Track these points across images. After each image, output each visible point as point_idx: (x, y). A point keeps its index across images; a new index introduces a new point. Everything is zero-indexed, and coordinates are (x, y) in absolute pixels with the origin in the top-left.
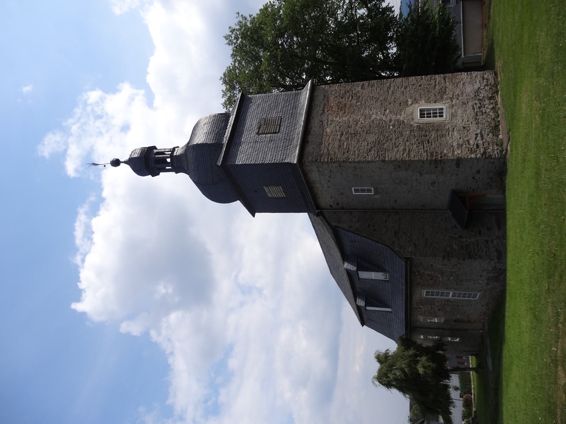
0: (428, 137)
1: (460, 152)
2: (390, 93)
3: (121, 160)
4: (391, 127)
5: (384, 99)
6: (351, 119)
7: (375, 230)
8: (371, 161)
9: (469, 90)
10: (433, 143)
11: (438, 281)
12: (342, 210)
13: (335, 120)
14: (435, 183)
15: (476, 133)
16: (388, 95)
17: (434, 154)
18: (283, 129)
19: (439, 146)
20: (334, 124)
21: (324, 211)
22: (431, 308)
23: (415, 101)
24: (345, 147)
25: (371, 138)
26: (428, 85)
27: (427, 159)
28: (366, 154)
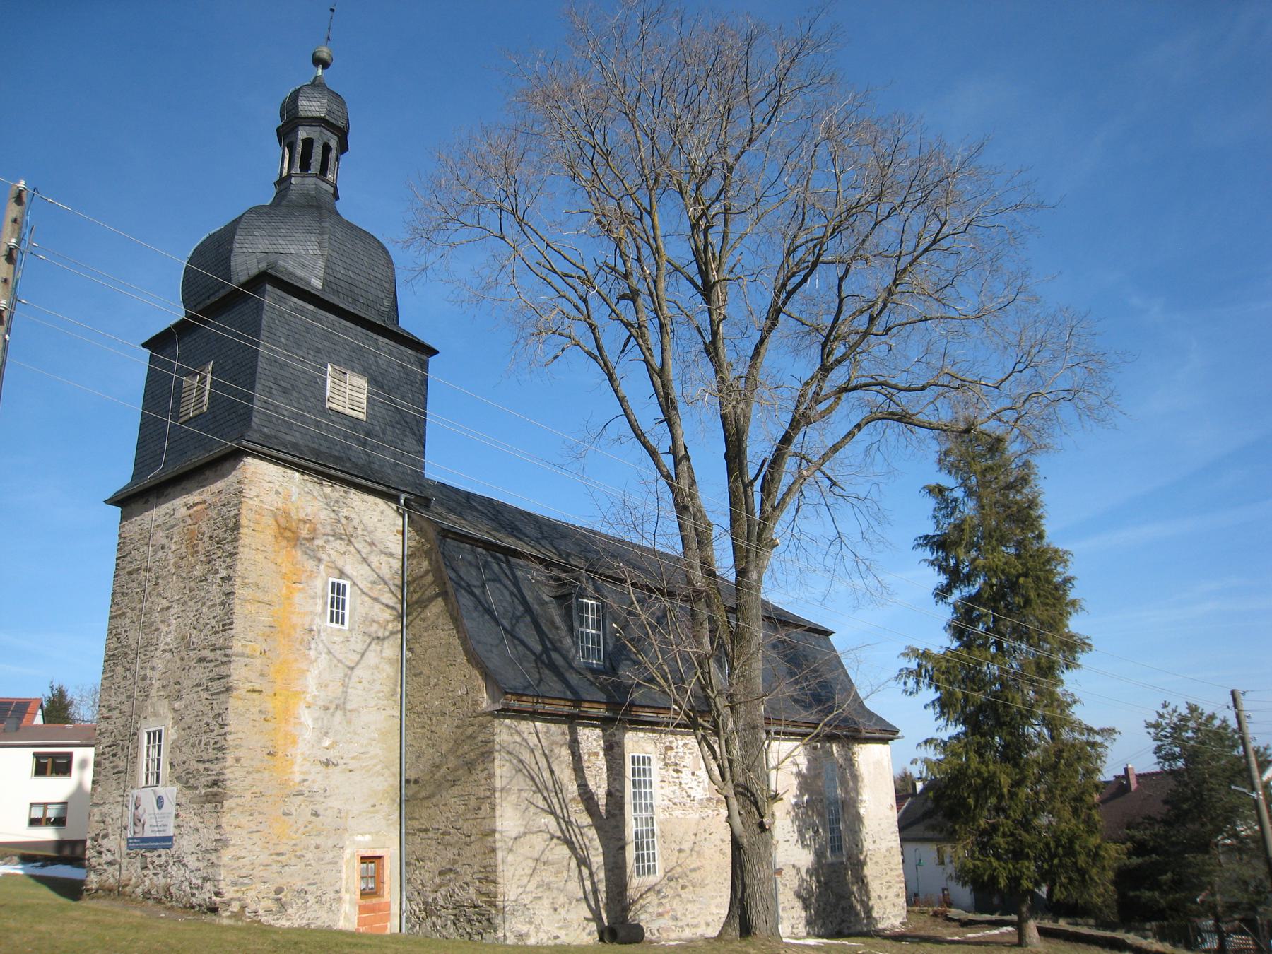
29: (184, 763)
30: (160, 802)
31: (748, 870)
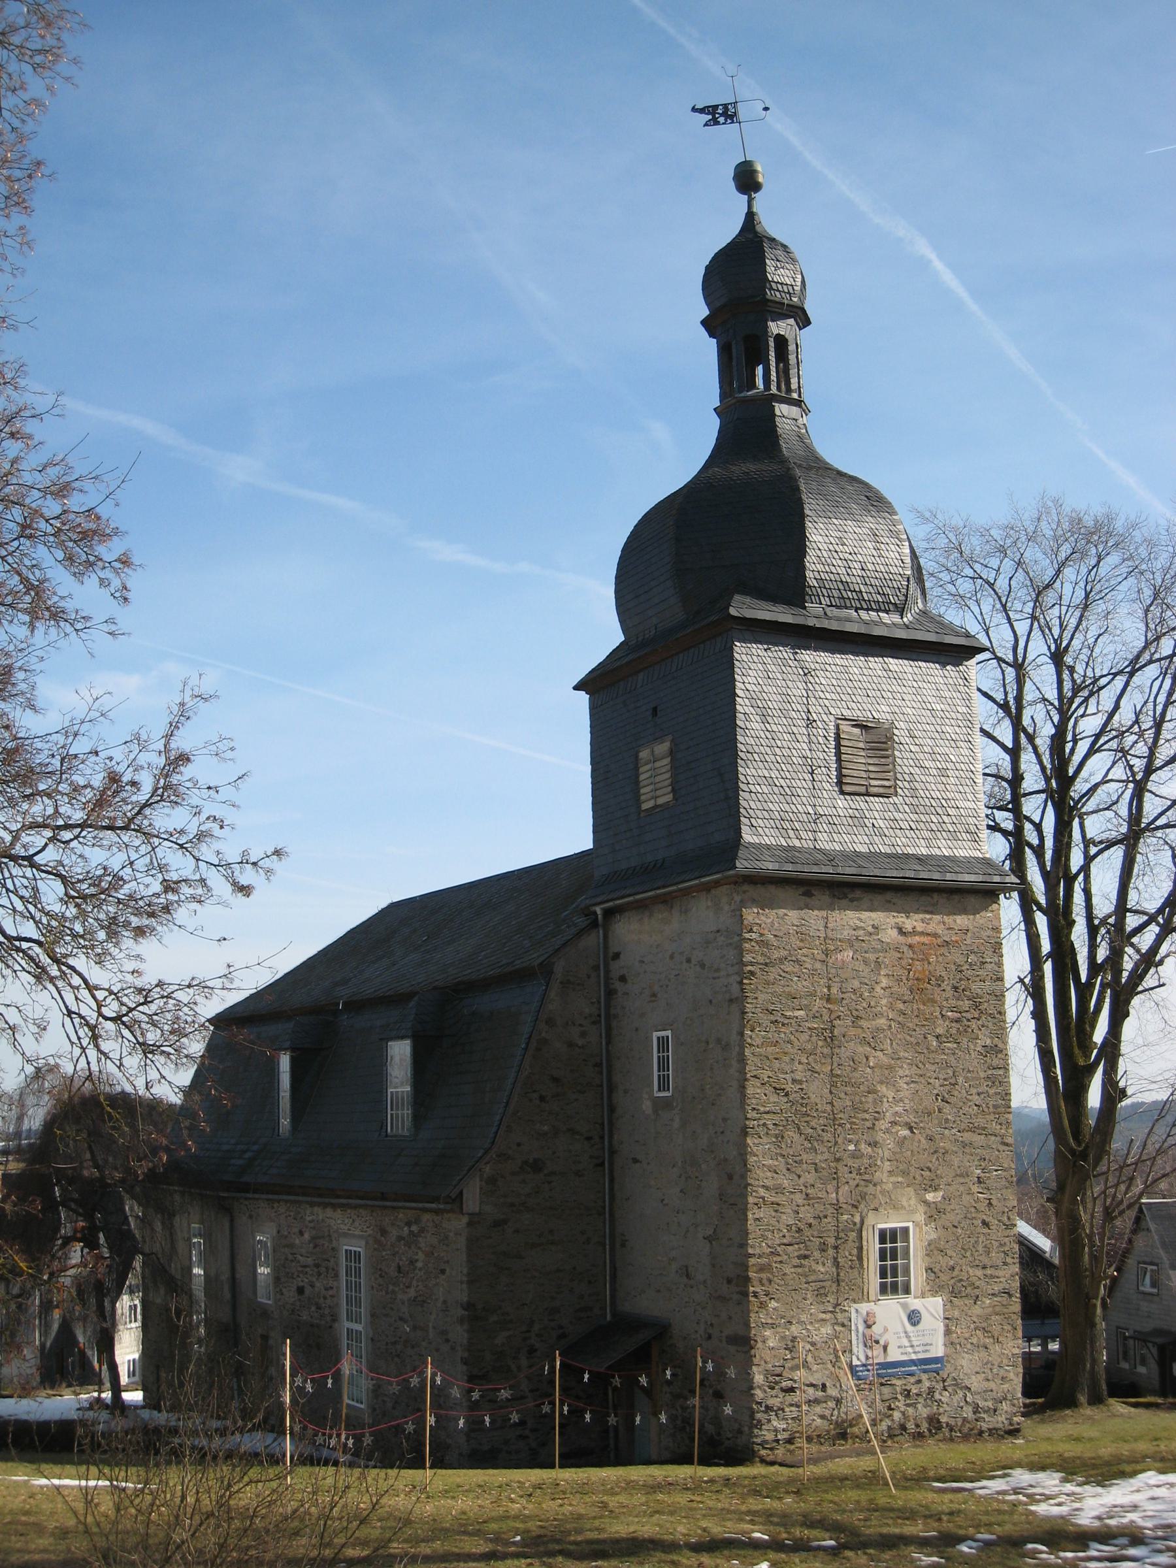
0: (817, 1254)
1: (771, 1345)
2: (966, 1134)
3: (758, 196)
4: (852, 1147)
5: (947, 1120)
6: (882, 1022)
7: (542, 1098)
8: (743, 1095)
9: (964, 1363)
10: (800, 1270)
11: (397, 1289)
12: (605, 991)
13: (879, 974)
14: (688, 1276)
15: (828, 1384)
16: (959, 1131)
17: (764, 1276)
18: (853, 807)
19: (790, 1288)
20: (865, 971)
21: (601, 932)
22: (305, 1267)
23: (934, 1213)
24: (788, 1014)
25: (817, 1091)
26: (985, 1247)
27: (751, 1256)
28: (766, 1079)
29: (953, 1269)
30: (914, 1318)
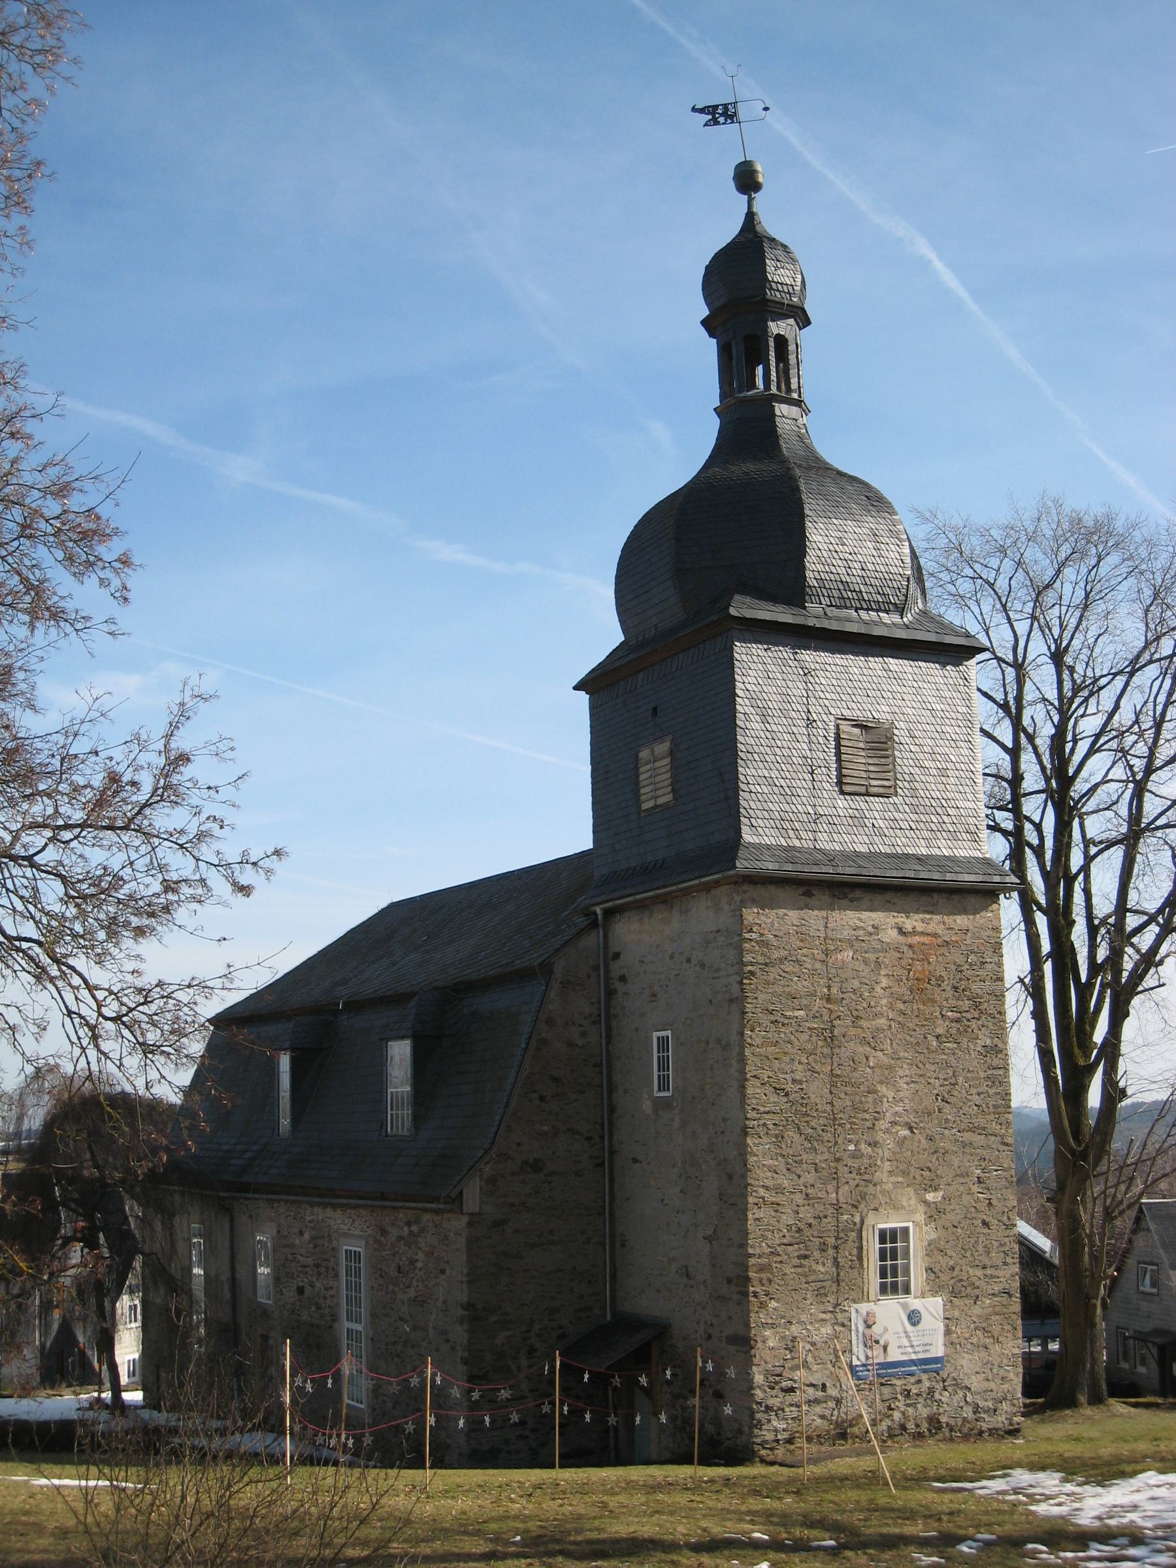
0: (817, 1254)
1: (771, 1345)
2: (966, 1134)
3: (758, 196)
4: (852, 1147)
5: (947, 1120)
6: (882, 1022)
7: (542, 1098)
8: (743, 1095)
9: (964, 1363)
10: (800, 1270)
11: (397, 1289)
12: (605, 991)
13: (879, 974)
14: (688, 1276)
15: (828, 1384)
16: (959, 1131)
17: (764, 1276)
18: (853, 807)
19: (790, 1288)
20: (865, 971)
21: (601, 932)
22: (305, 1267)
23: (934, 1213)
24: (788, 1014)
25: (817, 1091)
26: (985, 1247)
27: (751, 1256)
28: (766, 1079)
29: (953, 1269)
30: (914, 1318)
31: (363, 1212)
